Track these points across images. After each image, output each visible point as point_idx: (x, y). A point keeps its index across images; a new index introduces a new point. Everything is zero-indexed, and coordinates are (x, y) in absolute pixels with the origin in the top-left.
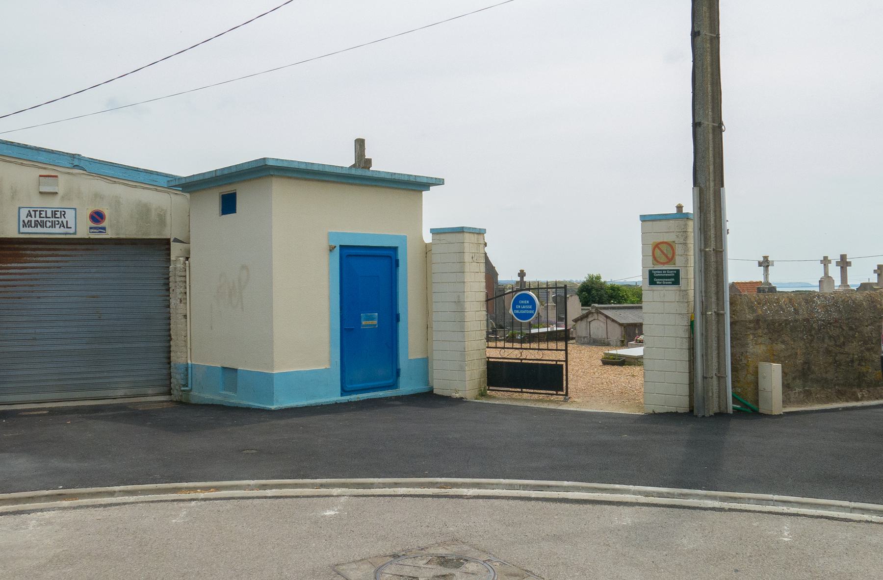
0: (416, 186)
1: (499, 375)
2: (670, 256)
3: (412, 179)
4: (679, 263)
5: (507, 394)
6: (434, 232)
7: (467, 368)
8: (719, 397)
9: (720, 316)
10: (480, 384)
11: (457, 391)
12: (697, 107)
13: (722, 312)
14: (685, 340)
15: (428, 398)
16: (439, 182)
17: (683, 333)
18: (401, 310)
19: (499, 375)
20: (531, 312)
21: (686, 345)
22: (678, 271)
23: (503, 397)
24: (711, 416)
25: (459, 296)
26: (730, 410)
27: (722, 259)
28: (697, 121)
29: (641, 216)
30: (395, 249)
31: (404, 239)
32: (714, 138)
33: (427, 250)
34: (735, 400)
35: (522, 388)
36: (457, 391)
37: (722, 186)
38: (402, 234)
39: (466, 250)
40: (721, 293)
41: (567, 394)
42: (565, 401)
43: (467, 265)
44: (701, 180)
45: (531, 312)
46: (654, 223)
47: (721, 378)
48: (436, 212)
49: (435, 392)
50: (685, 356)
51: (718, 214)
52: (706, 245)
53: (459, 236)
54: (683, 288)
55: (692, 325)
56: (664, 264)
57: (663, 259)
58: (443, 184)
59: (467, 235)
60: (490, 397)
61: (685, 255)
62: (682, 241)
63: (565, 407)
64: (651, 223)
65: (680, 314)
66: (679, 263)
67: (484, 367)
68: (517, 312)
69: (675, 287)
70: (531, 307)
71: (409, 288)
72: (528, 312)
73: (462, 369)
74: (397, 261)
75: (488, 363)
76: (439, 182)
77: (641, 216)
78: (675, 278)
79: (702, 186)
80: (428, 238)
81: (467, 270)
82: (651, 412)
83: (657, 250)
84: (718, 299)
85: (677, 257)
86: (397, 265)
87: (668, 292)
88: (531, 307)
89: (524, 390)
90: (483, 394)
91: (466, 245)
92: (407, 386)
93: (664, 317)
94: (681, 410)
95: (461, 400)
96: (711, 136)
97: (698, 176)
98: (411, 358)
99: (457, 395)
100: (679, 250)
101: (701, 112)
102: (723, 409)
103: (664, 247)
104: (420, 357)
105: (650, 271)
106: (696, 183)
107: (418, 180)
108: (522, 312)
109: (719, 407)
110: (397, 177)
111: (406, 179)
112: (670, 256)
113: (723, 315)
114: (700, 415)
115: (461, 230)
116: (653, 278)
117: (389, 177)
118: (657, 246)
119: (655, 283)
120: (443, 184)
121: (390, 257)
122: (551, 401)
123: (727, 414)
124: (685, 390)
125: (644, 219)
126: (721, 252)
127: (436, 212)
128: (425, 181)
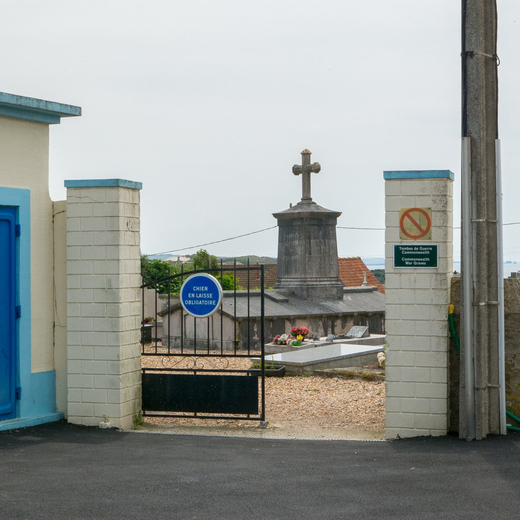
0: (40, 115)
1: (160, 393)
2: (424, 227)
3: (42, 106)
4: (435, 238)
5: (169, 420)
6: (70, 185)
7: (121, 385)
8: (489, 414)
9: (492, 308)
10: (134, 408)
11: (106, 419)
12: (468, 31)
13: (494, 302)
14: (443, 340)
15: (59, 428)
16: (74, 112)
17: (440, 330)
18: (22, 302)
19: (160, 393)
20: (211, 303)
21: (444, 346)
22: (435, 248)
23: (170, 424)
24: (484, 439)
25: (109, 281)
26: (504, 431)
27: (495, 233)
28: (467, 49)
29: (385, 173)
30: (15, 209)
31: (26, 194)
32: (487, 74)
33: (56, 212)
34: (509, 418)
35: (195, 412)
36: (106, 419)
37: (497, 138)
38: (23, 187)
39: (121, 214)
40: (493, 277)
41: (263, 418)
42: (263, 427)
43: (122, 234)
44: (472, 128)
45: (211, 303)
46: (403, 182)
47: (492, 390)
48: (68, 157)
49: (70, 420)
50: (443, 360)
51: (413, 175)
52: (479, 216)
53: (110, 193)
54: (440, 271)
55: (454, 322)
56: (415, 238)
57: (415, 232)
58: (80, 114)
59: (122, 192)
60: (148, 425)
61: (445, 226)
62: (440, 208)
63: (268, 435)
64: (397, 183)
65: (437, 305)
66: (435, 238)
67: (138, 383)
68: (190, 302)
69: (430, 270)
70: (210, 296)
71: (32, 267)
72: (206, 303)
73: (115, 387)
74: (17, 228)
75: (144, 377)
76: (74, 112)
77: (385, 173)
78: (430, 257)
79: (475, 136)
80: (58, 193)
81: (122, 242)
82: (395, 437)
83: (406, 219)
84: (489, 286)
85: (433, 229)
86: (18, 233)
87: (421, 276)
88: (210, 296)
89: (198, 414)
90: (138, 422)
91: (121, 205)
92: (30, 414)
93: (414, 309)
94: (436, 433)
95: (114, 430)
96: (483, 71)
97: (469, 123)
98: (33, 371)
99: (109, 424)
100: (436, 219)
101: (474, 39)
102: (494, 429)
103: (415, 215)
104: (44, 370)
105: (397, 248)
106: (465, 132)
107: (50, 108)
108: (197, 303)
109: (490, 428)
110: (23, 102)
111: (35, 105)
112: (424, 227)
113: (496, 306)
114: (470, 438)
115: (115, 184)
116: (401, 257)
117: (13, 101)
118: (406, 214)
119: (403, 264)
120: (80, 114)
121: (9, 222)
122: (239, 428)
123: (500, 435)
124: (441, 406)
125: (390, 176)
126: (495, 223)
127: (68, 157)
128: (57, 109)
